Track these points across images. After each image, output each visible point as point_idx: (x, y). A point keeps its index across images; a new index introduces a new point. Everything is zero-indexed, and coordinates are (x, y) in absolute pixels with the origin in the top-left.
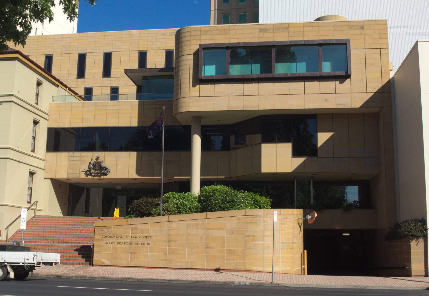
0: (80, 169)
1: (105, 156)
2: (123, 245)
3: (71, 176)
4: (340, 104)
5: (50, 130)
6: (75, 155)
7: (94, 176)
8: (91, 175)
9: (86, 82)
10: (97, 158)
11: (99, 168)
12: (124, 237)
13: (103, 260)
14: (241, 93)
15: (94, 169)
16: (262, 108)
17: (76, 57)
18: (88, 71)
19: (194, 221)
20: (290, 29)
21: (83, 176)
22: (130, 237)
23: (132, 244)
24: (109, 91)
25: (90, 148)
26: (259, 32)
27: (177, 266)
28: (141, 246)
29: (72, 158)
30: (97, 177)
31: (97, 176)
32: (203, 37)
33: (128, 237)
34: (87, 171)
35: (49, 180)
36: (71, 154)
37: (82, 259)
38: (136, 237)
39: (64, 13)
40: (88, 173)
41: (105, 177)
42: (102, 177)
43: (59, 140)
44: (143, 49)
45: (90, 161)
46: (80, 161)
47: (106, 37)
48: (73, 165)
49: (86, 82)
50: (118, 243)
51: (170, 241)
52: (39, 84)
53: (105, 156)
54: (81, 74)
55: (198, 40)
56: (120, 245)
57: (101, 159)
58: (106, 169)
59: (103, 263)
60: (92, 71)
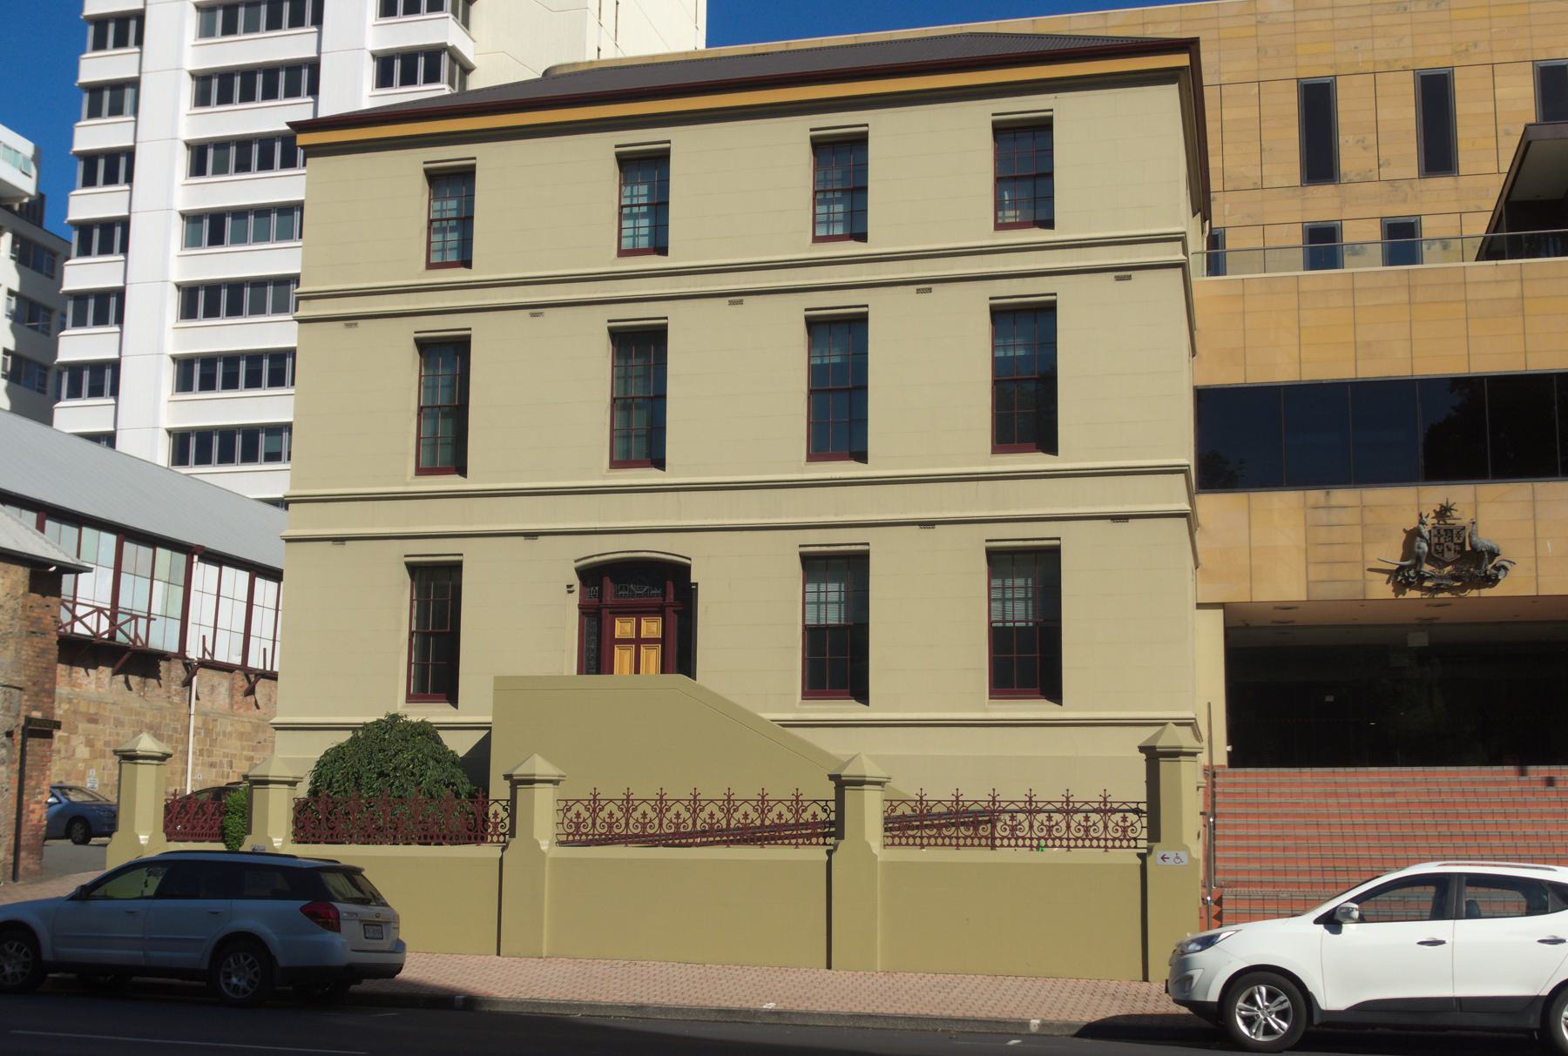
0: (1364, 562)
1: (1476, 503)
3: (1323, 593)
6: (1333, 502)
7: (1438, 589)
8: (1420, 588)
15: (1431, 559)
21: (1381, 589)
24: (1296, 237)
29: (1322, 515)
30: (1446, 595)
31: (1450, 589)
34: (1401, 568)
36: (1316, 495)
37: (172, 790)
39: (289, 124)
40: (1401, 578)
41: (1486, 592)
42: (1474, 593)
44: (1316, 70)
45: (1412, 523)
46: (1364, 525)
48: (1322, 549)
53: (1476, 503)
57: (1462, 516)
58: (1493, 554)
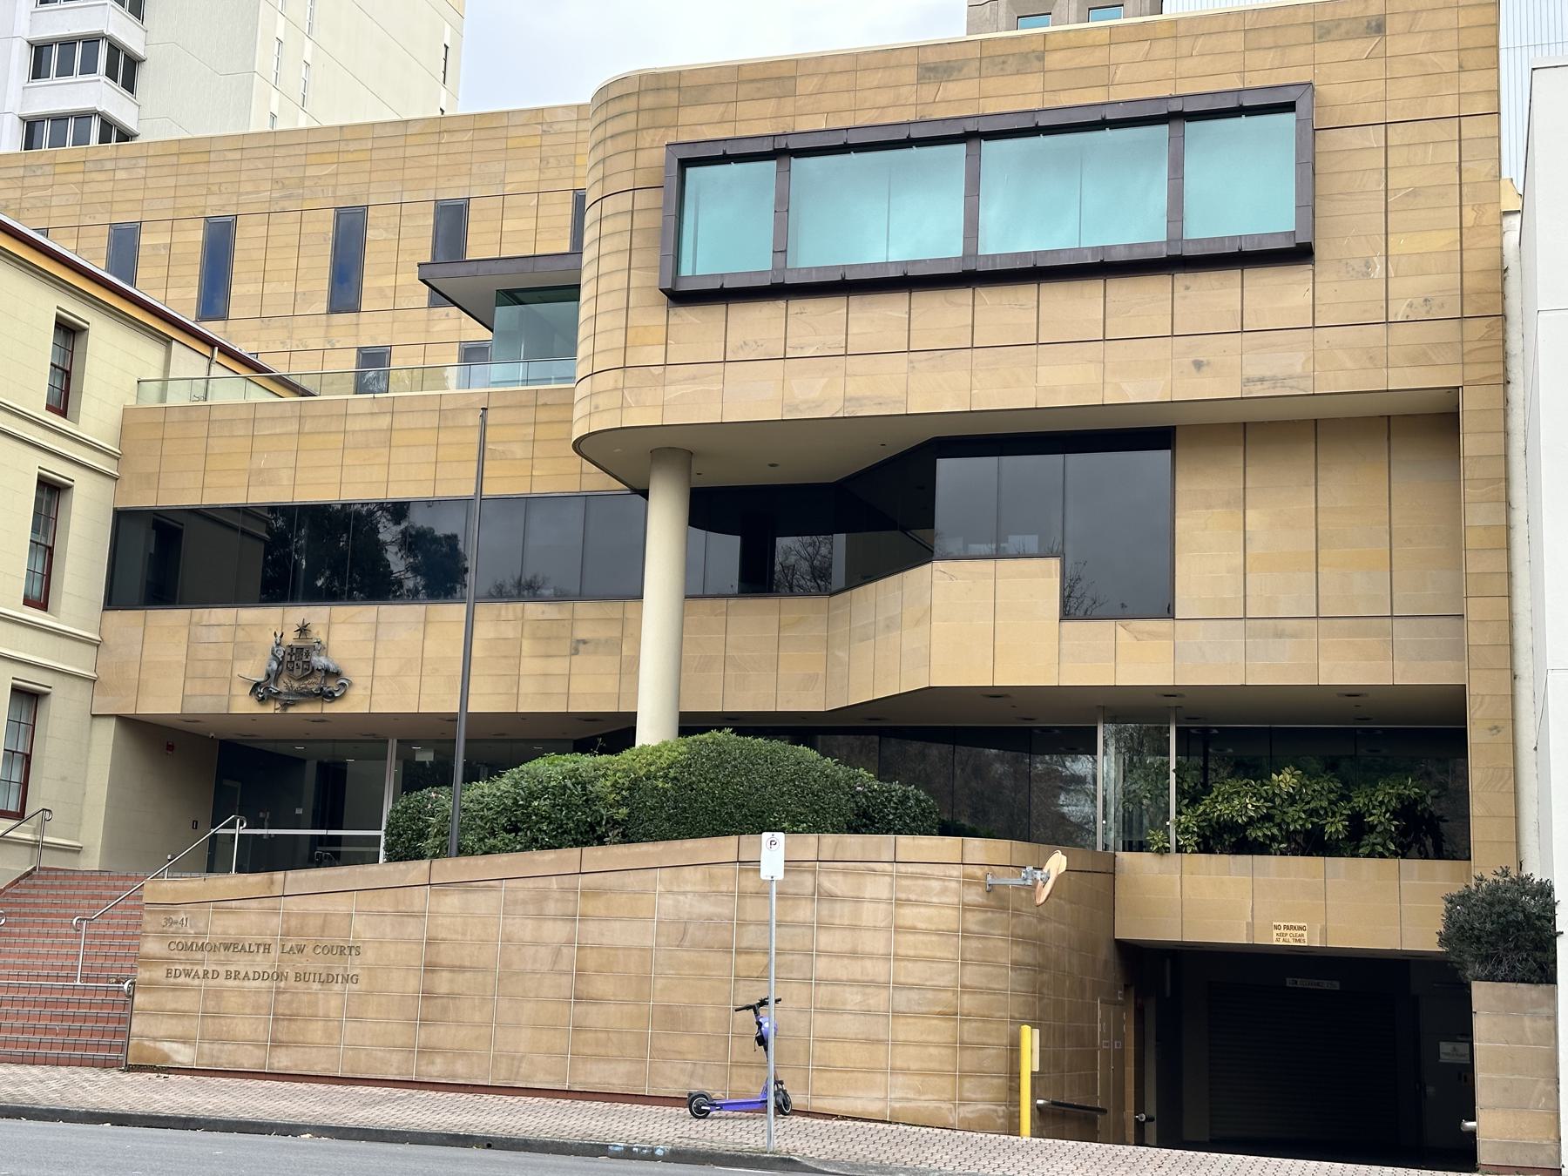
1: (330, 623)
2: (246, 983)
4: (1262, 380)
5: (122, 517)
9: (370, 329)
10: (303, 630)
11: (300, 667)
12: (254, 948)
13: (166, 1046)
14: (835, 341)
16: (918, 405)
17: (324, 225)
18: (374, 281)
19: (530, 883)
20: (1053, 60)
22: (275, 952)
23: (280, 976)
24: (350, 362)
25: (278, 587)
26: (921, 80)
27: (454, 1077)
28: (316, 986)
32: (688, 115)
33: (267, 948)
35: (113, 722)
38: (301, 950)
40: (260, 691)
43: (164, 558)
47: (446, 138)
49: (370, 329)
50: (228, 975)
51: (431, 968)
52: (68, 332)
53: (330, 623)
54: (345, 290)
55: (668, 127)
56: (237, 983)
57: (318, 633)
59: (167, 1058)
60: (389, 281)
